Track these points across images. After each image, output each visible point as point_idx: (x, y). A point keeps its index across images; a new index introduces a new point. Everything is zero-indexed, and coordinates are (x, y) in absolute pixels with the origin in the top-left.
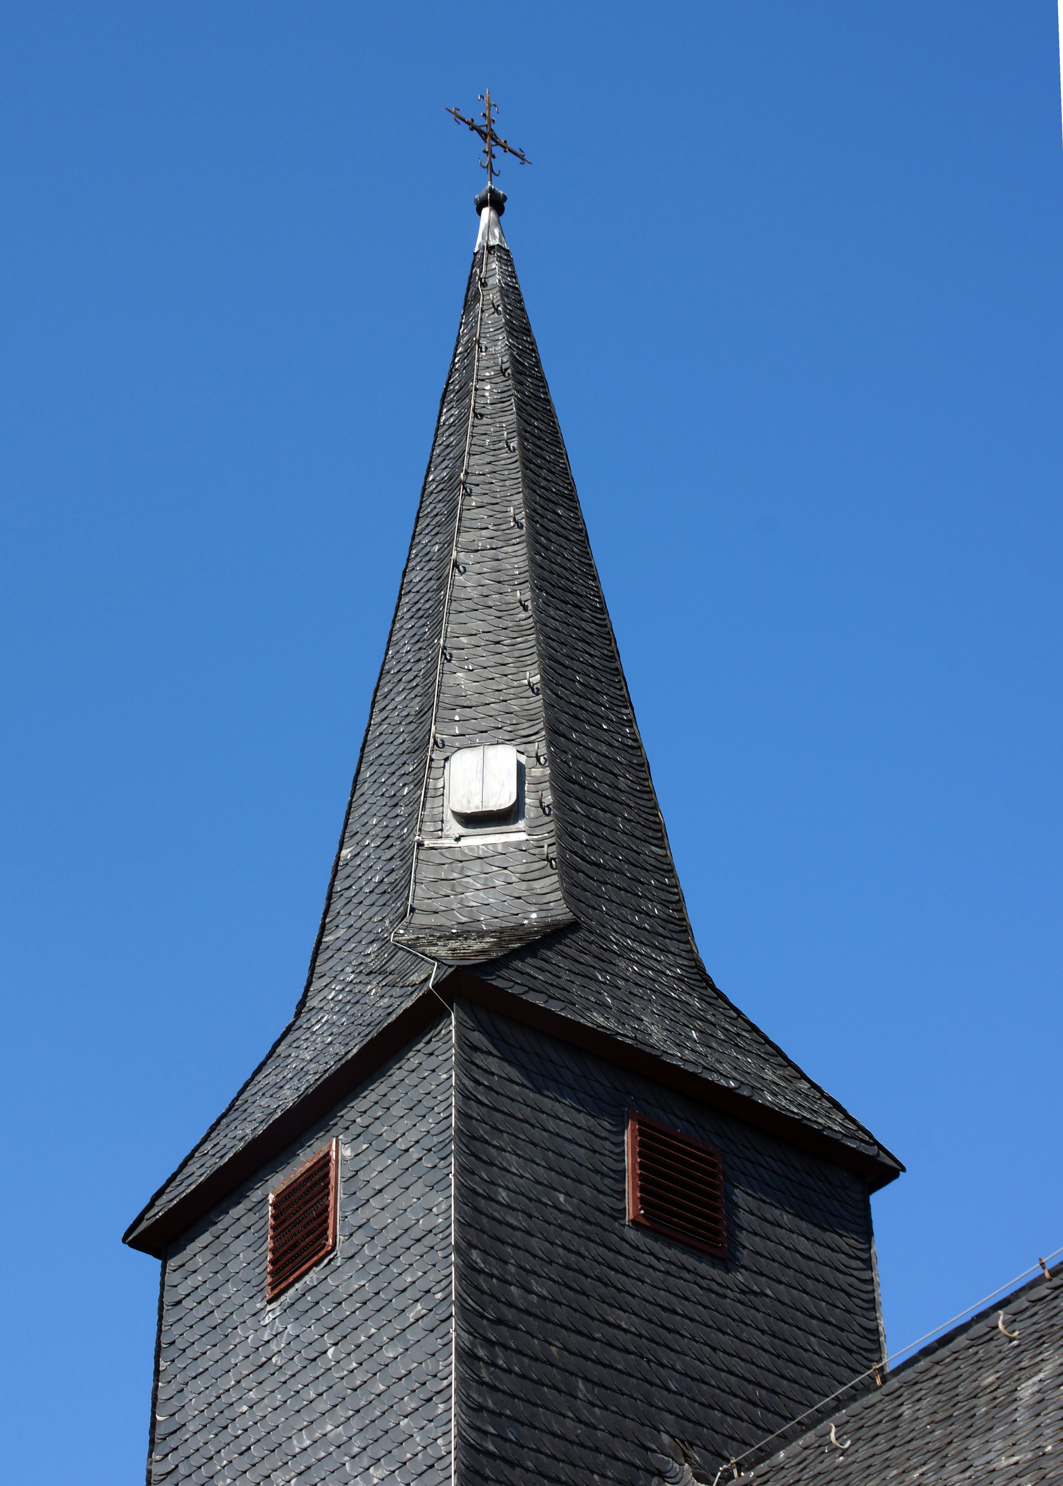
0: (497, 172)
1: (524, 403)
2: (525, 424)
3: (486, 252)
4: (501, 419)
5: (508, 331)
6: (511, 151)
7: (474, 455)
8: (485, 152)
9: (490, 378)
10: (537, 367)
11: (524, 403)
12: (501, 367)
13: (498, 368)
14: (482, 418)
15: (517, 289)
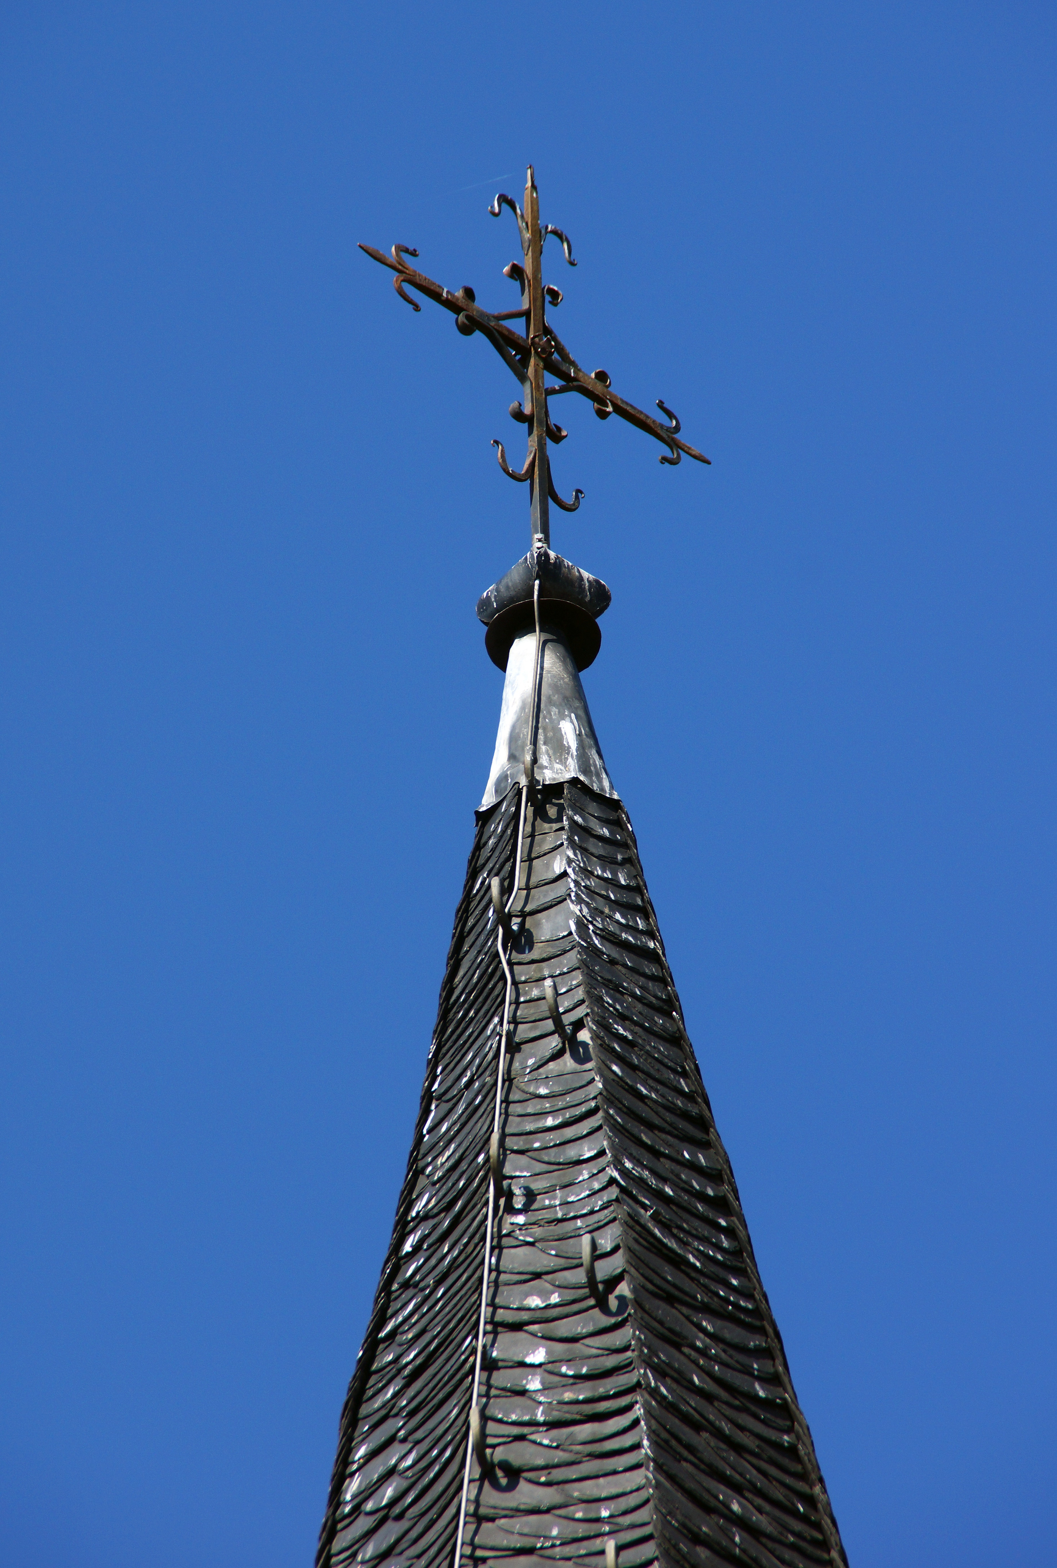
0: (567, 496)
1: (686, 1419)
2: (690, 1507)
3: (526, 811)
4: (590, 1489)
5: (617, 1129)
6: (623, 412)
7: (492, 1520)
8: (519, 416)
9: (544, 1316)
10: (740, 1272)
11: (686, 1419)
12: (591, 1273)
13: (579, 1276)
14: (511, 1486)
15: (653, 957)
